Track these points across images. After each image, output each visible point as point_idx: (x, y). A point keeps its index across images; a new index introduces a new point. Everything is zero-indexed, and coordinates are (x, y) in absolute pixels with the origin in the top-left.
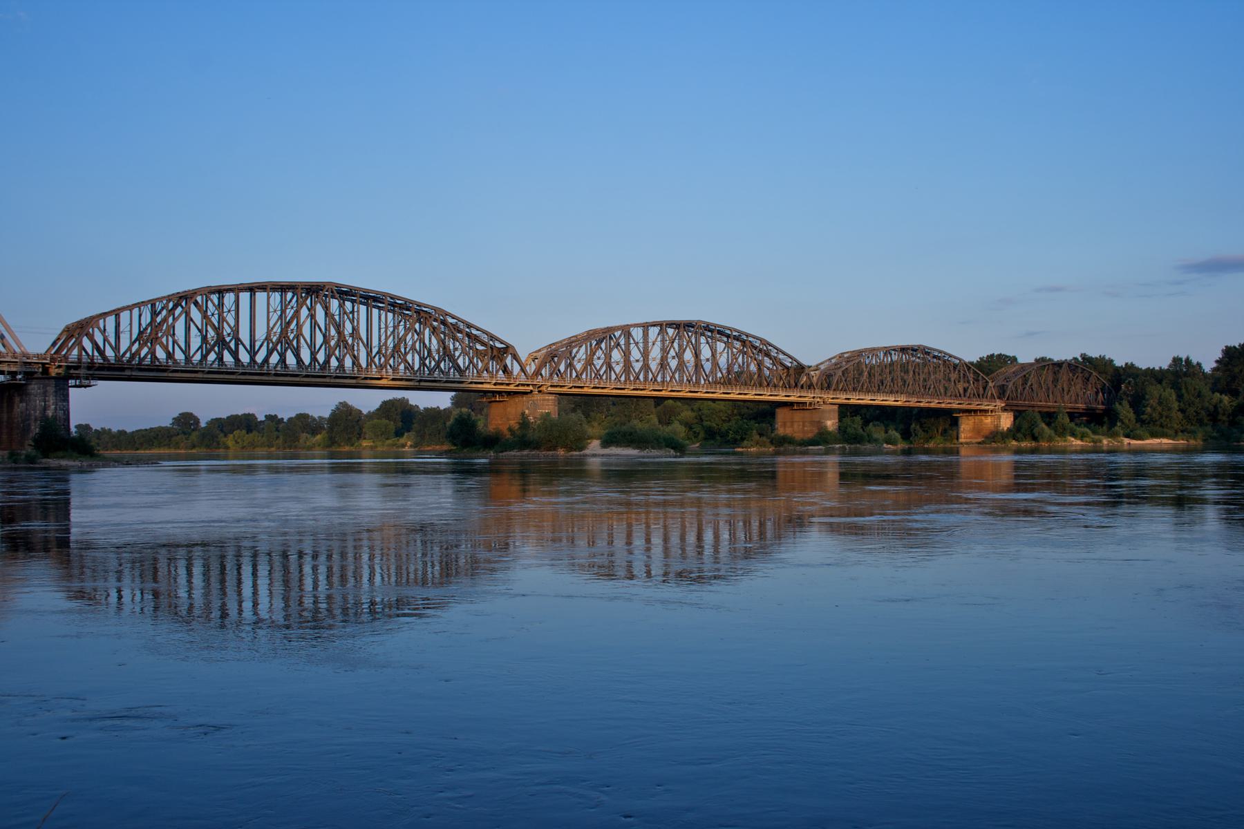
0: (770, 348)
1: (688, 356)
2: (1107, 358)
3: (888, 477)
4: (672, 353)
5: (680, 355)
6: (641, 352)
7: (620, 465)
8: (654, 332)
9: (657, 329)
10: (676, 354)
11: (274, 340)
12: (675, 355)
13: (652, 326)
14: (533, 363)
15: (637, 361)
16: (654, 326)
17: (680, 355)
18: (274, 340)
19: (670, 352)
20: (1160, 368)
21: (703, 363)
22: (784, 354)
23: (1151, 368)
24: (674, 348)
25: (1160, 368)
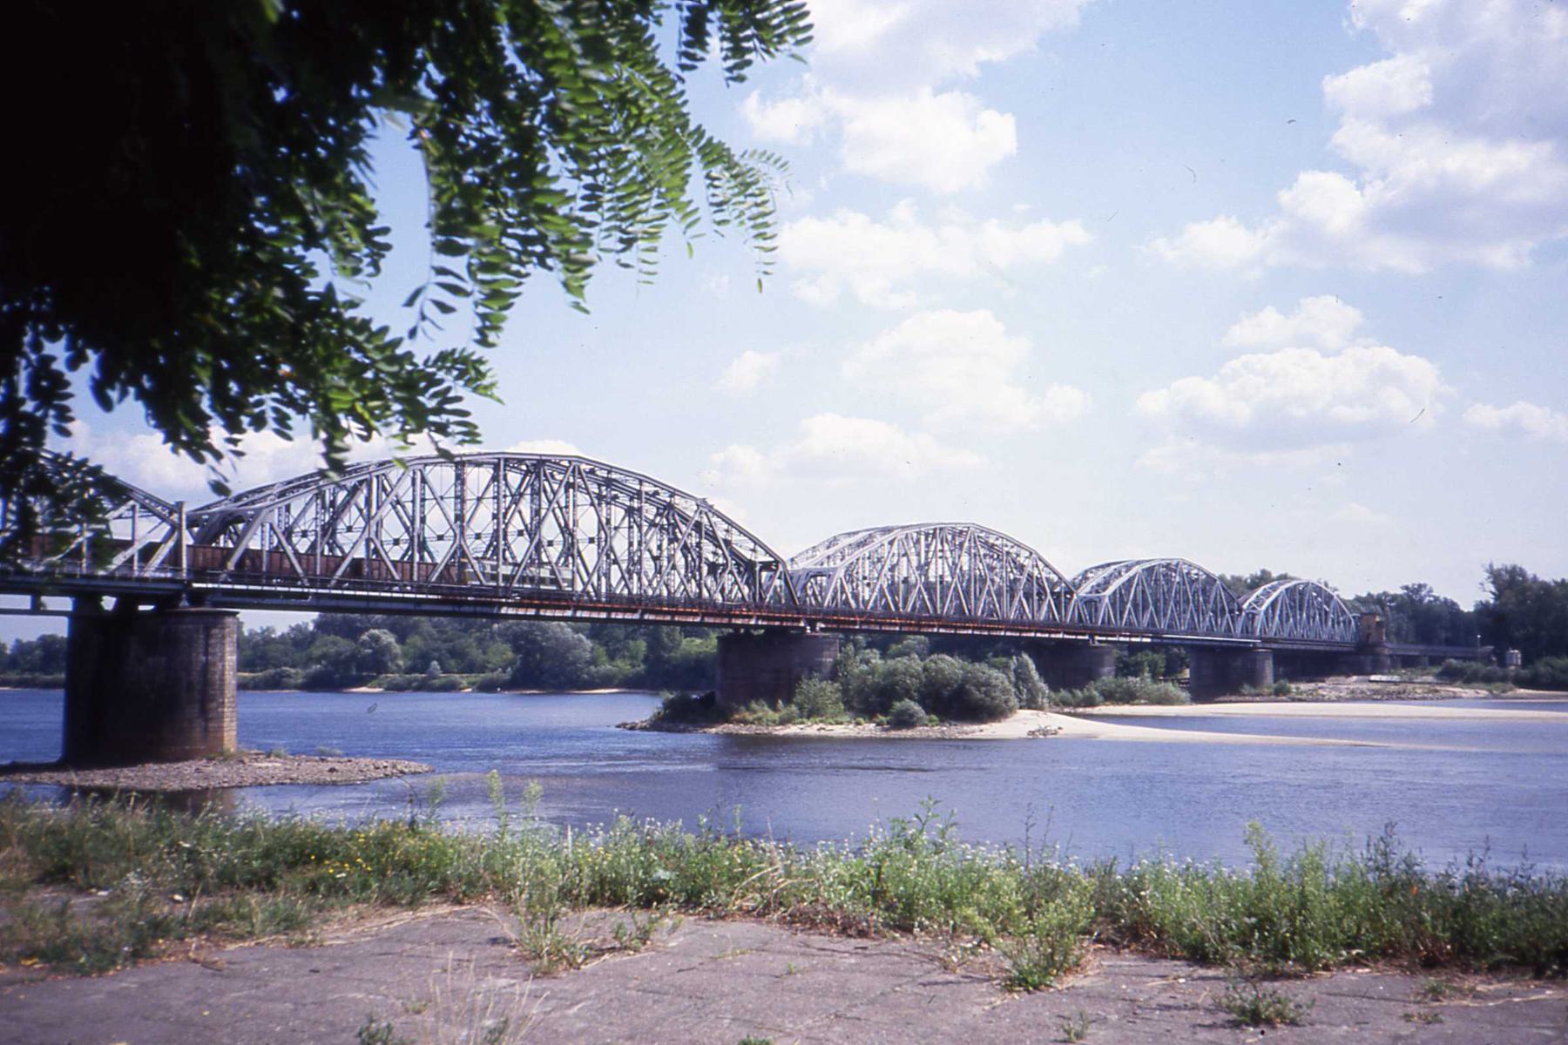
0: (714, 519)
1: (550, 530)
2: (1442, 598)
3: (1317, 732)
4: (516, 524)
5: (532, 531)
6: (559, 525)
7: (788, 770)
8: (478, 478)
9: (487, 473)
10: (526, 526)
11: (354, 511)
12: (522, 527)
13: (471, 463)
14: (711, 558)
15: (440, 538)
16: (479, 464)
17: (532, 531)
18: (354, 511)
19: (513, 522)
20: (165, 442)
21: (581, 547)
22: (742, 532)
23: (726, 146)
24: (520, 512)
25: (165, 442)
